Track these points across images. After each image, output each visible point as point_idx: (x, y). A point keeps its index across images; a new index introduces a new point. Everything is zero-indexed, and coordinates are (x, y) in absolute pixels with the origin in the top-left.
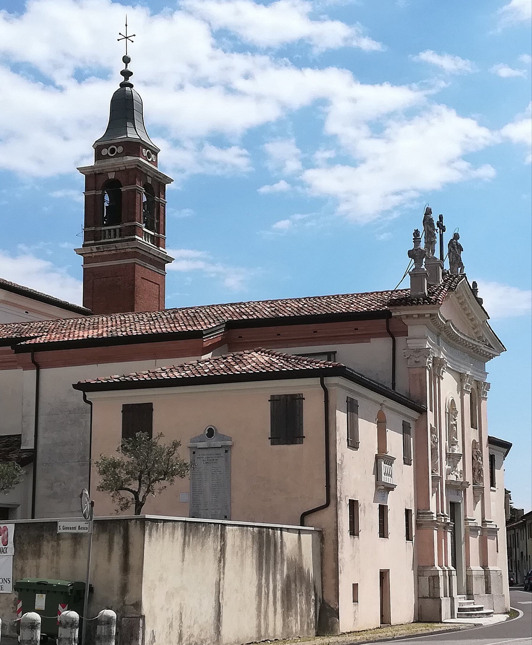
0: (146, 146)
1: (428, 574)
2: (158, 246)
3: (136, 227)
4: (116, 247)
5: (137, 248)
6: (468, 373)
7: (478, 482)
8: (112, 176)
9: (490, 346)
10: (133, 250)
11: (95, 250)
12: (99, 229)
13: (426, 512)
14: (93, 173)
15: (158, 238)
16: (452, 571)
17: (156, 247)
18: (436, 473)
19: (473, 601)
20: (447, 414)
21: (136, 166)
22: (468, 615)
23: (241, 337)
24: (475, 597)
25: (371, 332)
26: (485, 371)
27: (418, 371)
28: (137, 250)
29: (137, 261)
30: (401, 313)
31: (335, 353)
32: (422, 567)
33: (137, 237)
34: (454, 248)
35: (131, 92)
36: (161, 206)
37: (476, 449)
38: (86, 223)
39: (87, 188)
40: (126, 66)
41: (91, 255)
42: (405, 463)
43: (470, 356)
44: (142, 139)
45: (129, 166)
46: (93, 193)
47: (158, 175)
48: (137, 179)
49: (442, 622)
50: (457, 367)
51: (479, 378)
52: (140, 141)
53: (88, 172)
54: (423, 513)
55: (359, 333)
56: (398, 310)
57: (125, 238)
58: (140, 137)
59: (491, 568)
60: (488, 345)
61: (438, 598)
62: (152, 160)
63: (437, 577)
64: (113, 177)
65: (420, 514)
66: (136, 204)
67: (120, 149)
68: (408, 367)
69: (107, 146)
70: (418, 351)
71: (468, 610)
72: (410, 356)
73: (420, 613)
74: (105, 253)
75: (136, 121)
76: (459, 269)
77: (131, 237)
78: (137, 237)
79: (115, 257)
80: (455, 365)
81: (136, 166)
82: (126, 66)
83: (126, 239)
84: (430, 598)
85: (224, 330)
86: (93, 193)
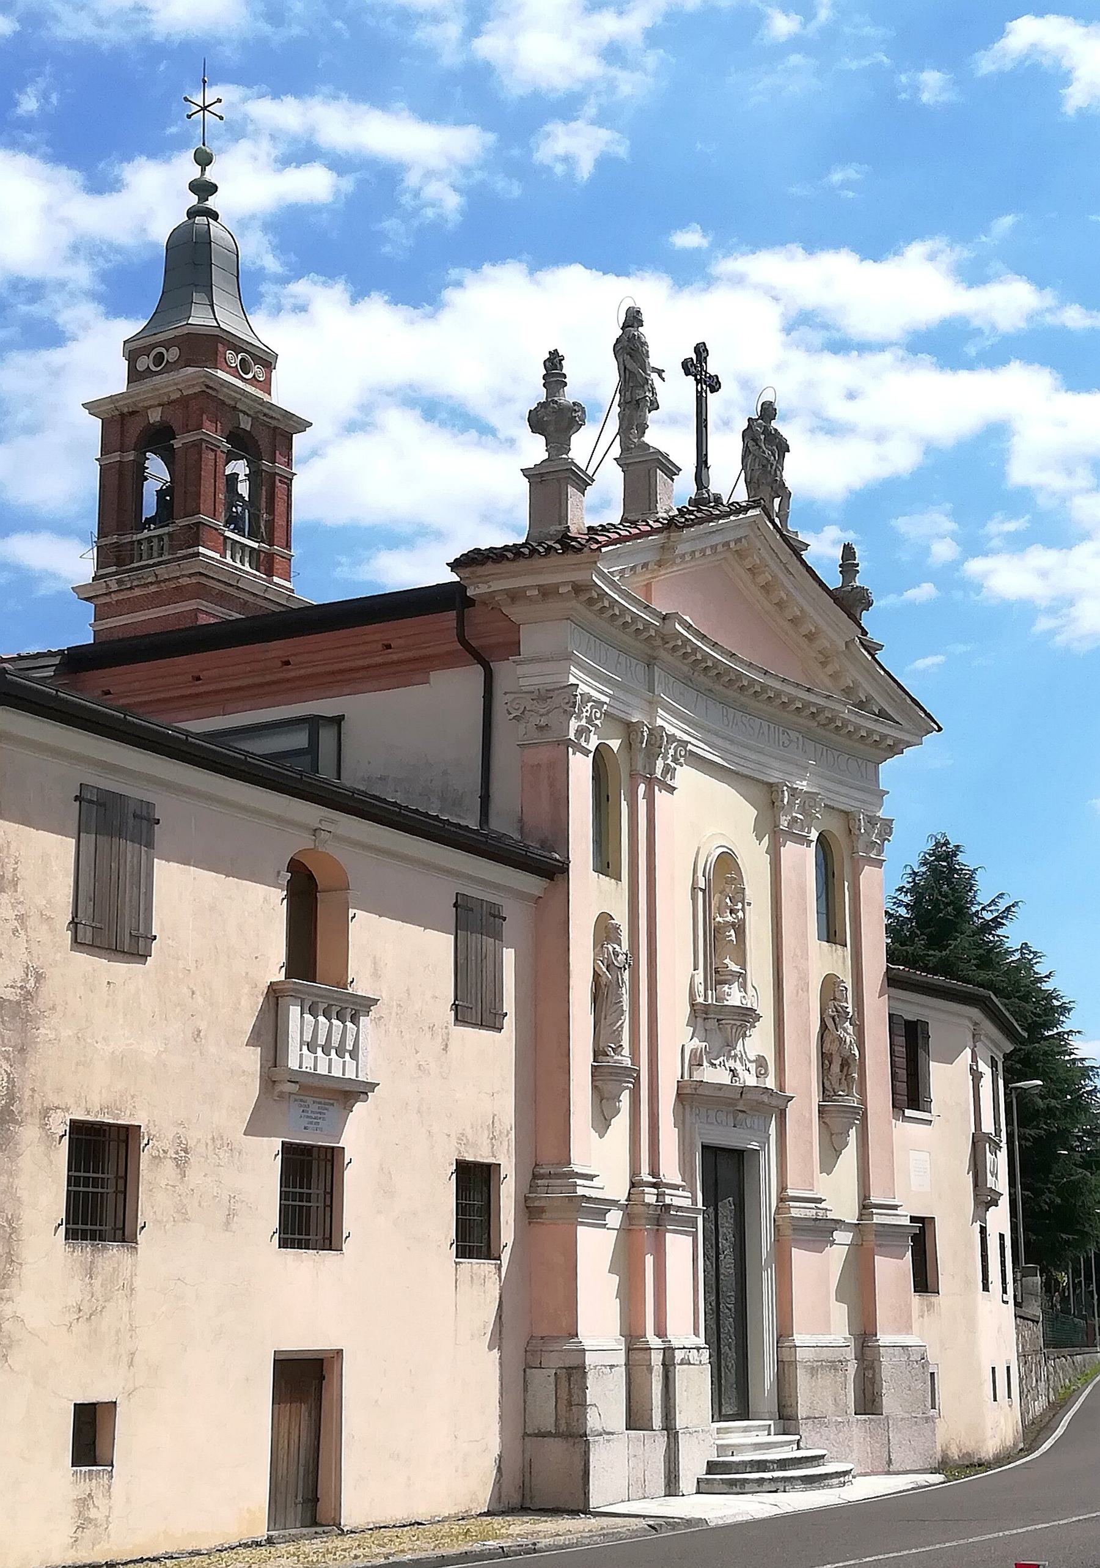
0: (236, 345)
1: (554, 1361)
2: (270, 573)
3: (201, 527)
4: (156, 576)
5: (201, 574)
6: (803, 785)
7: (841, 1093)
8: (155, 416)
9: (882, 714)
10: (194, 580)
11: (114, 587)
12: (127, 539)
13: (560, 1170)
14: (117, 413)
15: (270, 557)
16: (587, 1352)
17: (264, 576)
18: (616, 1057)
19: (798, 1437)
20: (700, 894)
21: (204, 388)
22: (732, 1483)
23: (108, 693)
24: (805, 1429)
25: (428, 652)
26: (879, 787)
27: (543, 755)
28: (203, 580)
29: (203, 606)
30: (490, 587)
31: (337, 721)
32: (542, 1338)
33: (201, 550)
34: (755, 440)
35: (207, 226)
36: (277, 482)
37: (835, 999)
38: (102, 528)
39: (105, 450)
40: (203, 170)
41: (107, 599)
42: (460, 1019)
43: (808, 735)
44: (221, 326)
45: (189, 387)
46: (116, 457)
47: (266, 411)
48: (205, 417)
49: (590, 1513)
50: (752, 766)
51: (853, 803)
52: (217, 332)
53: (104, 411)
54: (550, 1175)
55: (395, 657)
56: (484, 579)
57: (178, 555)
58: (218, 323)
59: (884, 1338)
60: (877, 713)
61: (581, 1436)
62: (254, 376)
63: (581, 1370)
64: (158, 419)
65: (542, 1177)
66: (200, 474)
67: (172, 355)
68: (518, 745)
69: (145, 351)
70: (543, 696)
71: (741, 1469)
72: (523, 713)
73: (527, 1480)
74: (137, 592)
75: (216, 290)
76: (777, 501)
77: (191, 551)
78: (201, 550)
79: (156, 600)
80: (745, 758)
81: (204, 388)
82: (203, 170)
83: (181, 555)
84: (558, 1435)
85: (52, 673)
86: (116, 457)
